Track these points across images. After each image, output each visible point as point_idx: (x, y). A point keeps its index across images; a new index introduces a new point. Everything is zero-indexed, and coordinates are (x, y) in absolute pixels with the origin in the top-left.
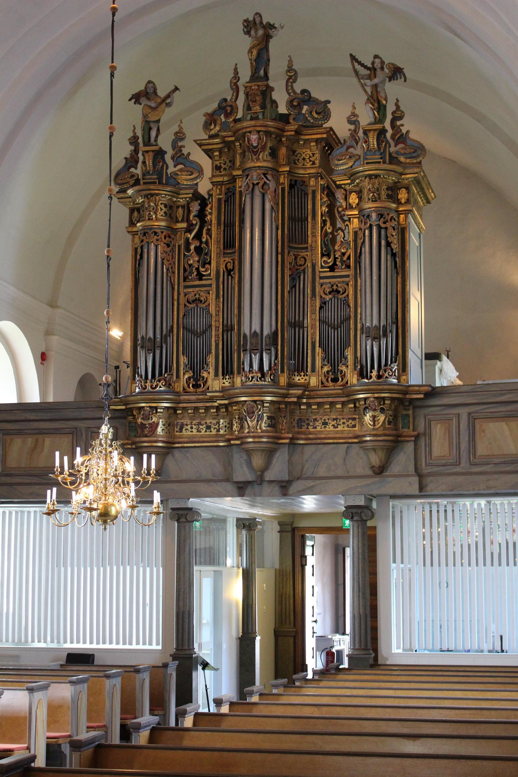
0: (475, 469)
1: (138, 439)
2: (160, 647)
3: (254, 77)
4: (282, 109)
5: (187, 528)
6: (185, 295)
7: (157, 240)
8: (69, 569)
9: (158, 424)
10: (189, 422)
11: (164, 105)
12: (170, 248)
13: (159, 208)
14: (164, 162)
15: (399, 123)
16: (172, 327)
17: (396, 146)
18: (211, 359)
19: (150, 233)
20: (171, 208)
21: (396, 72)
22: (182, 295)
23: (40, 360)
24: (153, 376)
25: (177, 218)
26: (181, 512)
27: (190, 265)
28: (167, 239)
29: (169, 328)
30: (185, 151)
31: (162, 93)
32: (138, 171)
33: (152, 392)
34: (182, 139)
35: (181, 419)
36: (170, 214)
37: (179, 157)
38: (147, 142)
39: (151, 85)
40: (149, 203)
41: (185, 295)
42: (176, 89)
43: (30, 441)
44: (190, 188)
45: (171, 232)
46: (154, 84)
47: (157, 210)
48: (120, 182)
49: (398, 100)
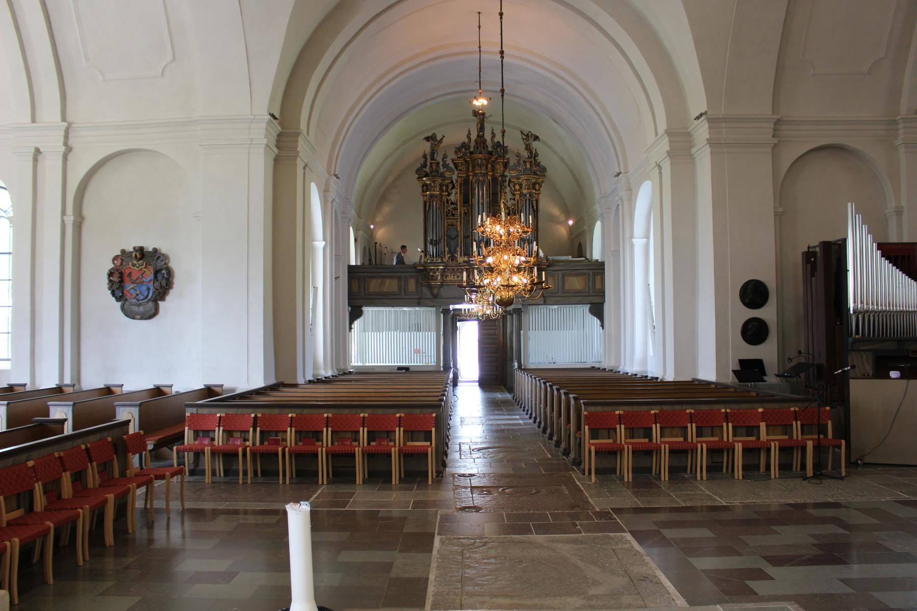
3: (478, 136)
4: (490, 149)
18: (459, 249)
20: (441, 186)
21: (536, 138)
31: (438, 138)
32: (427, 170)
38: (432, 158)
43: (379, 281)
45: (441, 195)
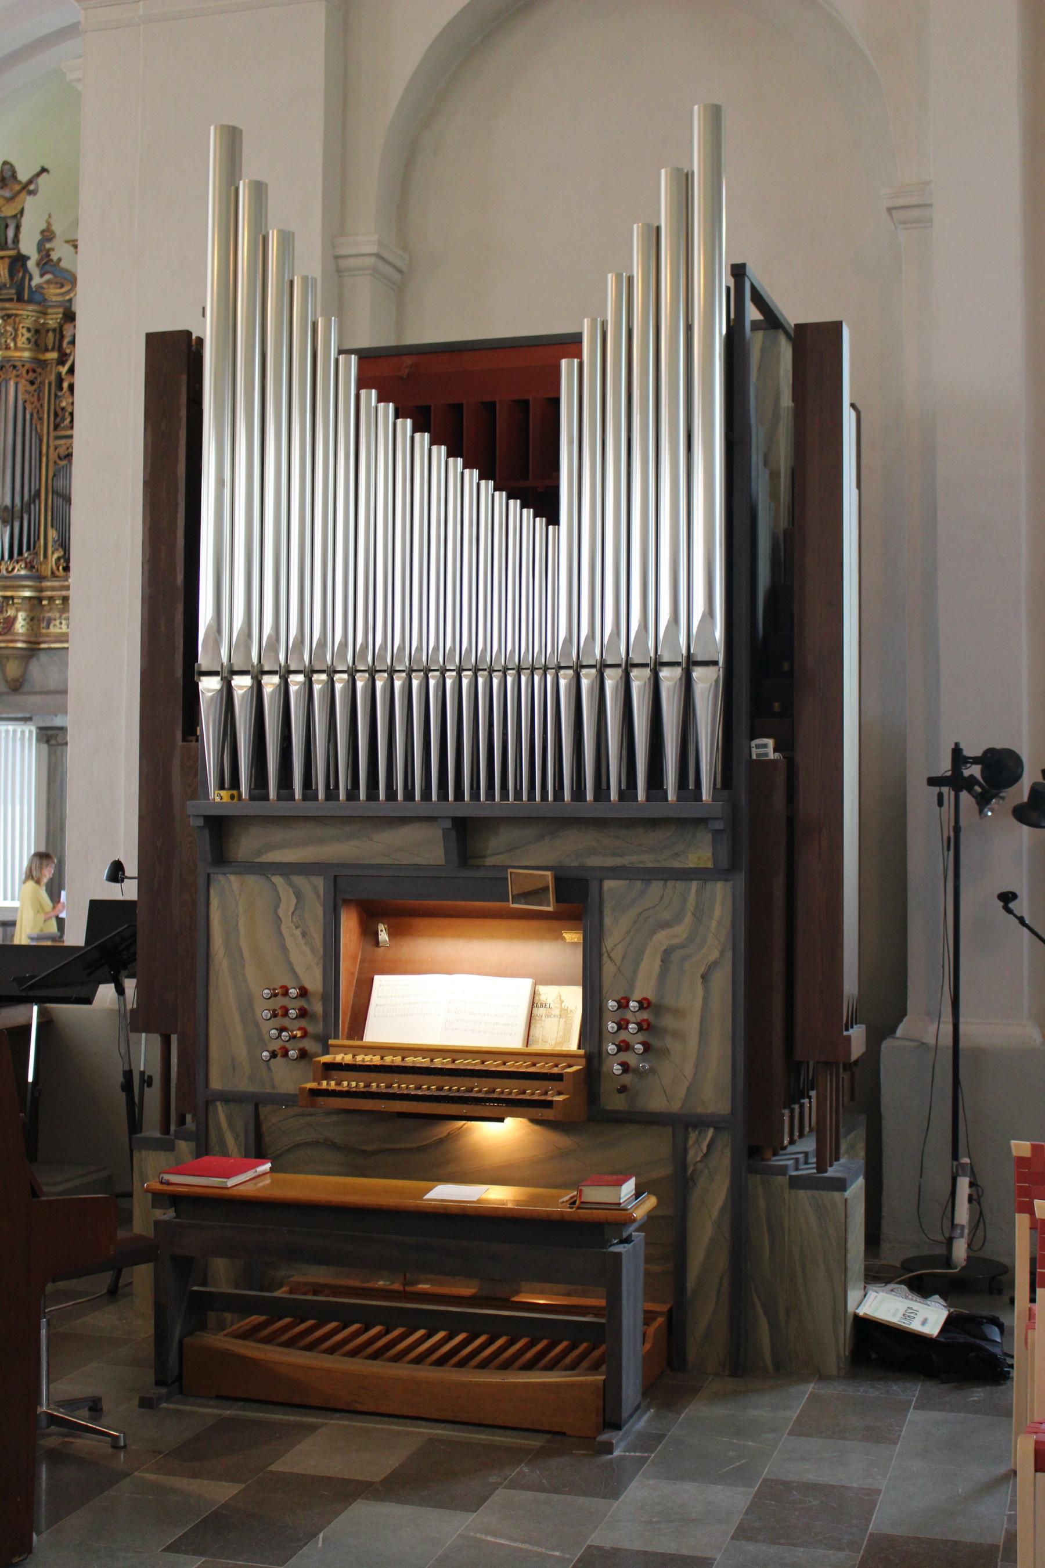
5: (59, 753)
6: (56, 449)
7: (17, 376)
9: (15, 618)
10: (58, 615)
11: (24, 194)
12: (35, 386)
13: (19, 333)
14: (26, 270)
15: (48, 246)
16: (39, 492)
17: (42, 276)
19: (8, 366)
20: (38, 332)
22: (52, 449)
24: (11, 557)
25: (46, 346)
26: (50, 732)
27: (63, 409)
28: (31, 374)
29: (33, 492)
30: (54, 256)
31: (23, 176)
33: (6, 578)
34: (50, 239)
35: (49, 612)
36: (36, 342)
37: (45, 263)
39: (7, 167)
40: (4, 327)
41: (56, 449)
42: (44, 170)
44: (59, 306)
46: (12, 166)
49: (50, 216)
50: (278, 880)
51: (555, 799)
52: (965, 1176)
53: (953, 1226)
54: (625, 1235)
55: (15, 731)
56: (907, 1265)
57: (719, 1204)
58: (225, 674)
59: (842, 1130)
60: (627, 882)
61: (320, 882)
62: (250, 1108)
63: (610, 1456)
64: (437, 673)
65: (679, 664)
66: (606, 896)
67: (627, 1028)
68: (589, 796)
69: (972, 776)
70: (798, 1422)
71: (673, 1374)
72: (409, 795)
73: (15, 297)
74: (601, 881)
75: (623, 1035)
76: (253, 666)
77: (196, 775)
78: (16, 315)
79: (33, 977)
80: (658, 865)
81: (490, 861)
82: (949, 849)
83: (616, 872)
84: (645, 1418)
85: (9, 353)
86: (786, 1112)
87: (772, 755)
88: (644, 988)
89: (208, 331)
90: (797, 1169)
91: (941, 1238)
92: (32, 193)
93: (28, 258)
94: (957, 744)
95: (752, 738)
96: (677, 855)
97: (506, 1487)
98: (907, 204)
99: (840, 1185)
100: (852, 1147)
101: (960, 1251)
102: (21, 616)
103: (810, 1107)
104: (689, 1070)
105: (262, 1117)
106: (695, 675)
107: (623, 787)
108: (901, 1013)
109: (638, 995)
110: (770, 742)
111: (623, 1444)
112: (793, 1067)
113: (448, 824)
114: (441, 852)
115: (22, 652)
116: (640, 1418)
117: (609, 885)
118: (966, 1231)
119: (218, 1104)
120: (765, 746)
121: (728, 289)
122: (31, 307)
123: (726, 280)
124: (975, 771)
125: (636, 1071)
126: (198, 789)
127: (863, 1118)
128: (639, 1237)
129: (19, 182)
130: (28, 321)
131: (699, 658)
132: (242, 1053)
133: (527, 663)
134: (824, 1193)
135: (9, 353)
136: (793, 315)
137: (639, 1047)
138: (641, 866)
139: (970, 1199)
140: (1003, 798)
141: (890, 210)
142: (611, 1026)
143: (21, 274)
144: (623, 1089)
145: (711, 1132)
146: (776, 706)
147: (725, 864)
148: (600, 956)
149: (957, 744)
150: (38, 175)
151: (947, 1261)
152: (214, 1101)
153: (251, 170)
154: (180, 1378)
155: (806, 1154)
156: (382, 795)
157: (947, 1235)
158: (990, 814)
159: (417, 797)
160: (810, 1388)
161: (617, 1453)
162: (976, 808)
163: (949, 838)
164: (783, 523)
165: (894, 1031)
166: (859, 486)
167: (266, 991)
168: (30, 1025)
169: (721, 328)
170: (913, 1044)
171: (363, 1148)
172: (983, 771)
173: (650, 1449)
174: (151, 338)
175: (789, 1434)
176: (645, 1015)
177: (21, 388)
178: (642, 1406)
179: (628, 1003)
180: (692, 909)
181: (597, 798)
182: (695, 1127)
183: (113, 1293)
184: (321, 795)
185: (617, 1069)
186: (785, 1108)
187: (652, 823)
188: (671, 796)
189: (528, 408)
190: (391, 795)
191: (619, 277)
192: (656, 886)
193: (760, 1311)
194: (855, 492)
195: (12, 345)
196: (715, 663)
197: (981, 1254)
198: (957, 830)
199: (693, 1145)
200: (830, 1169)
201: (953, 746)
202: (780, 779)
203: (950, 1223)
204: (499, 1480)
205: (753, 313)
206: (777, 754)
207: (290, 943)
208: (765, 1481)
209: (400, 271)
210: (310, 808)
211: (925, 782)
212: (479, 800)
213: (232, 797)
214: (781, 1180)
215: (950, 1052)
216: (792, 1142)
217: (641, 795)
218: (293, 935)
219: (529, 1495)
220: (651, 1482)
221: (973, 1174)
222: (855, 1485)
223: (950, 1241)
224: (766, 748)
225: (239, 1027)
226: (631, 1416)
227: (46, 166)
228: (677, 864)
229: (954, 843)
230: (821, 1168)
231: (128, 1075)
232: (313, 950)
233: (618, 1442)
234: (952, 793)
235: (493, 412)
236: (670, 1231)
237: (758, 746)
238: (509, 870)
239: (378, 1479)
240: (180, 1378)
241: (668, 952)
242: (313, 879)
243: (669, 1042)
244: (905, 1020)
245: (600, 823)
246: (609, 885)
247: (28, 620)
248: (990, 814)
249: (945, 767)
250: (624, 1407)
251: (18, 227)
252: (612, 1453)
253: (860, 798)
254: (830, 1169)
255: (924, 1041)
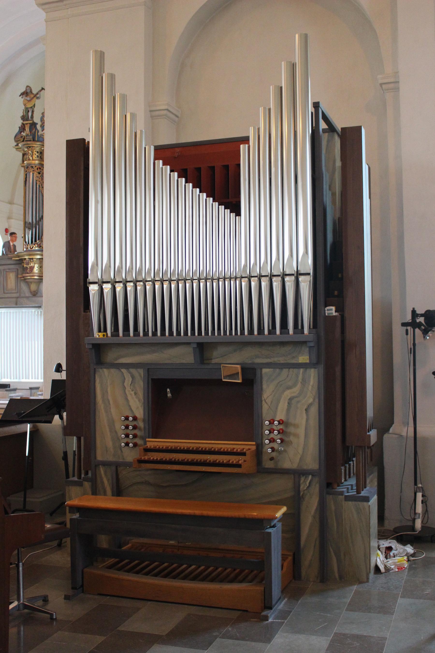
0: (6, 295)
1: (24, 275)
2: (42, 381)
7: (33, 171)
8: (33, 342)
11: (35, 98)
12: (40, 175)
23: (5, 233)
28: (39, 170)
31: (35, 92)
33: (30, 251)
36: (41, 157)
39: (28, 88)
42: (43, 89)
46: (30, 87)
47: (33, 155)
48: (17, 140)
50: (124, 370)
51: (241, 334)
52: (420, 492)
53: (415, 513)
54: (272, 524)
55: (35, 312)
56: (396, 530)
57: (315, 508)
58: (100, 283)
59: (367, 474)
60: (272, 370)
61: (141, 371)
62: (114, 468)
63: (267, 622)
64: (190, 281)
65: (293, 275)
66: (264, 375)
67: (273, 433)
68: (256, 332)
69: (420, 322)
70: (350, 604)
71: (295, 585)
72: (179, 333)
73: (32, 139)
74: (261, 369)
75: (272, 436)
76: (111, 279)
77: (89, 327)
78: (33, 147)
79: (24, 413)
80: (286, 362)
81: (214, 361)
82: (411, 353)
83: (268, 365)
84: (283, 603)
85: (30, 162)
86: (343, 468)
87: (334, 314)
88: (281, 415)
89: (91, 139)
90: (348, 492)
91: (409, 518)
92: (38, 98)
93: (37, 124)
94: (413, 309)
95: (326, 307)
96: (294, 357)
97: (220, 638)
98: (390, 81)
99: (367, 499)
100: (371, 481)
101: (418, 524)
102: (36, 266)
103: (353, 465)
104: (300, 451)
105: (119, 472)
106: (300, 279)
107: (270, 328)
108: (392, 423)
109: (278, 419)
110: (333, 308)
111: (273, 616)
112: (346, 448)
113: (195, 346)
114: (192, 358)
115: (38, 280)
116: (281, 603)
117: (265, 371)
118: (421, 516)
119: (101, 466)
120: (331, 310)
121: (312, 113)
122: (38, 143)
123: (311, 109)
124: (421, 320)
125: (278, 451)
126: (90, 332)
127: (376, 469)
128: (279, 525)
129: (33, 94)
130: (37, 149)
131: (302, 272)
132: (110, 444)
133: (228, 275)
134: (360, 503)
135: (30, 162)
136: (339, 125)
137: (279, 441)
138: (279, 362)
139: (422, 502)
140: (433, 331)
141: (381, 84)
142: (267, 432)
143: (34, 130)
144: (272, 459)
145: (310, 477)
146: (336, 293)
147: (314, 361)
148: (261, 401)
149: (413, 309)
150: (40, 91)
151: (413, 528)
152: (99, 465)
153: (108, 69)
154: (82, 586)
155: (352, 485)
156: (167, 334)
157: (413, 517)
158: (428, 338)
159: (182, 334)
160: (355, 587)
161: (270, 620)
162: (423, 335)
163: (411, 348)
164: (338, 215)
165: (389, 430)
166: (370, 198)
167: (123, 418)
168: (27, 432)
169: (309, 131)
170: (397, 436)
171: (162, 485)
172: (425, 320)
173: (284, 618)
174: (68, 142)
175: (346, 610)
176: (281, 427)
177: (35, 175)
178: (282, 598)
179: (274, 421)
180: (301, 381)
181: (259, 333)
182: (303, 475)
183: (60, 545)
184: (141, 334)
185: (270, 450)
186: (342, 466)
187: (283, 344)
188: (291, 332)
189: (228, 168)
190: (171, 333)
191: (265, 108)
192: (285, 371)
193: (333, 554)
194: (368, 200)
195: (31, 158)
196: (309, 274)
197: (427, 525)
198: (414, 345)
199: (303, 482)
200: (362, 492)
201: (412, 309)
202: (338, 324)
203: (414, 512)
204: (218, 634)
205: (323, 125)
206: (336, 313)
207: (129, 398)
208: (335, 633)
209: (177, 116)
210: (136, 340)
211: (400, 325)
212: (208, 335)
213: (104, 335)
214: (341, 497)
215: (413, 439)
216: (346, 480)
217: (278, 331)
218: (131, 394)
219: (231, 641)
220: (285, 634)
221: (423, 490)
222: (375, 635)
223: (414, 520)
224: (331, 311)
225: (109, 434)
226: (277, 603)
227: (43, 87)
228: (294, 361)
229: (413, 351)
230: (358, 492)
231: (65, 453)
232: (139, 400)
233: (271, 615)
234: (412, 329)
235: (214, 172)
236: (293, 522)
237: (328, 310)
238: (222, 365)
239: (164, 634)
240: (82, 586)
241: (291, 399)
242: (139, 370)
243: (292, 438)
244: (393, 425)
245: (261, 344)
246: (265, 371)
247: (39, 267)
248: (428, 338)
249: (409, 318)
250: (273, 600)
251: (33, 112)
252: (268, 620)
253: (373, 334)
254: (362, 492)
255: (402, 434)
